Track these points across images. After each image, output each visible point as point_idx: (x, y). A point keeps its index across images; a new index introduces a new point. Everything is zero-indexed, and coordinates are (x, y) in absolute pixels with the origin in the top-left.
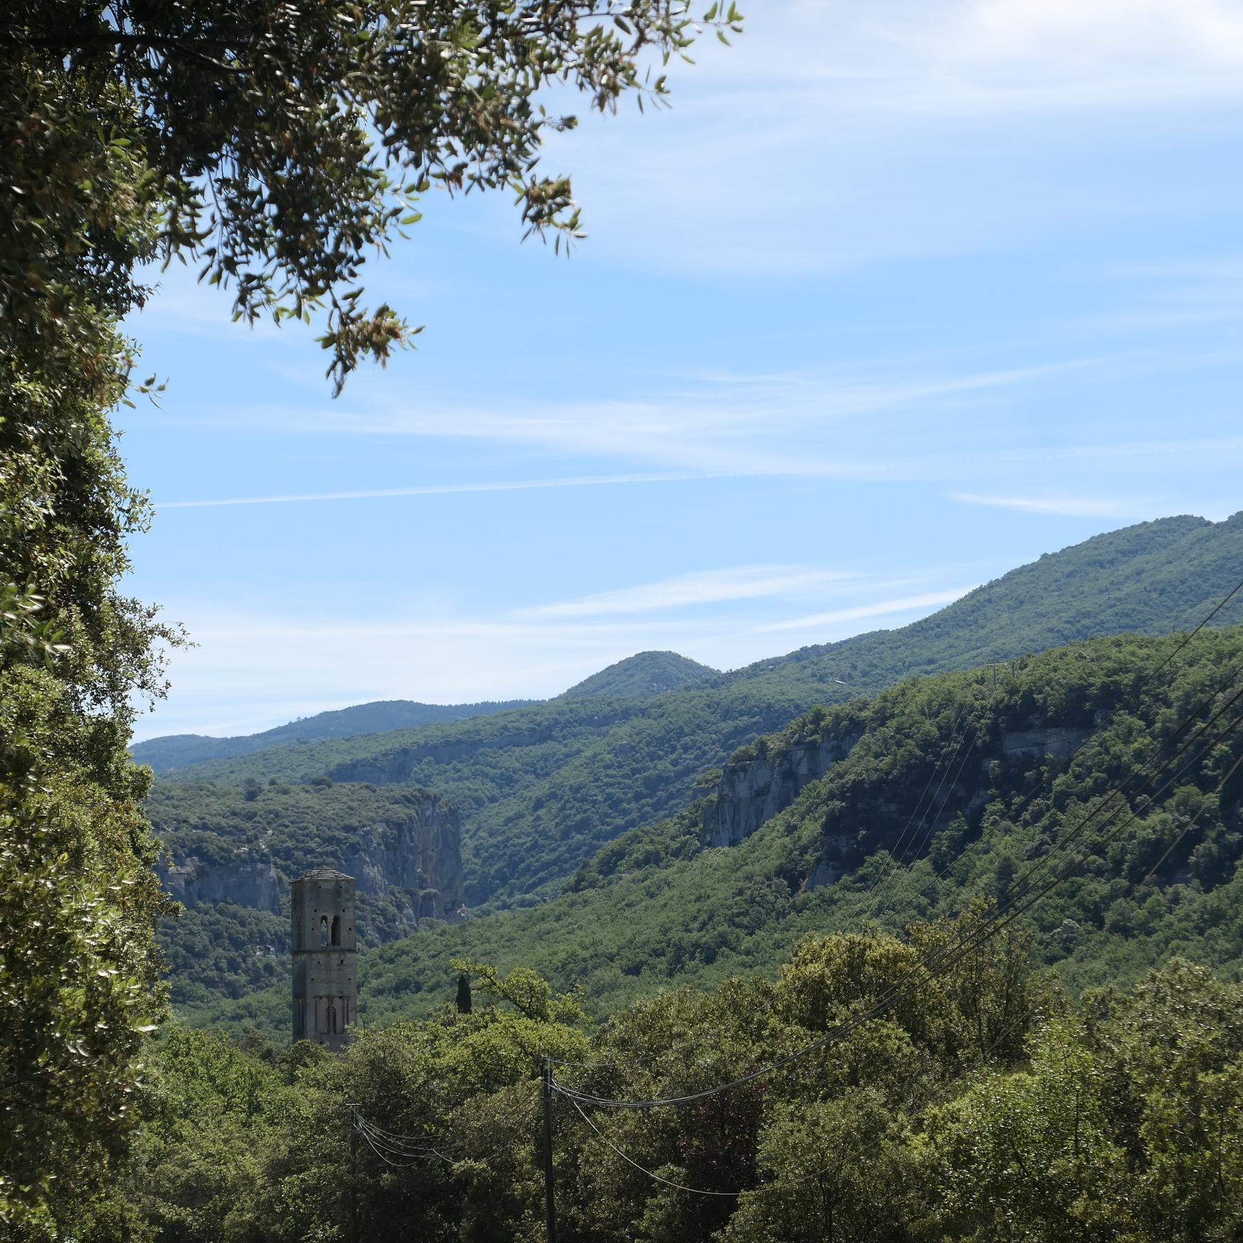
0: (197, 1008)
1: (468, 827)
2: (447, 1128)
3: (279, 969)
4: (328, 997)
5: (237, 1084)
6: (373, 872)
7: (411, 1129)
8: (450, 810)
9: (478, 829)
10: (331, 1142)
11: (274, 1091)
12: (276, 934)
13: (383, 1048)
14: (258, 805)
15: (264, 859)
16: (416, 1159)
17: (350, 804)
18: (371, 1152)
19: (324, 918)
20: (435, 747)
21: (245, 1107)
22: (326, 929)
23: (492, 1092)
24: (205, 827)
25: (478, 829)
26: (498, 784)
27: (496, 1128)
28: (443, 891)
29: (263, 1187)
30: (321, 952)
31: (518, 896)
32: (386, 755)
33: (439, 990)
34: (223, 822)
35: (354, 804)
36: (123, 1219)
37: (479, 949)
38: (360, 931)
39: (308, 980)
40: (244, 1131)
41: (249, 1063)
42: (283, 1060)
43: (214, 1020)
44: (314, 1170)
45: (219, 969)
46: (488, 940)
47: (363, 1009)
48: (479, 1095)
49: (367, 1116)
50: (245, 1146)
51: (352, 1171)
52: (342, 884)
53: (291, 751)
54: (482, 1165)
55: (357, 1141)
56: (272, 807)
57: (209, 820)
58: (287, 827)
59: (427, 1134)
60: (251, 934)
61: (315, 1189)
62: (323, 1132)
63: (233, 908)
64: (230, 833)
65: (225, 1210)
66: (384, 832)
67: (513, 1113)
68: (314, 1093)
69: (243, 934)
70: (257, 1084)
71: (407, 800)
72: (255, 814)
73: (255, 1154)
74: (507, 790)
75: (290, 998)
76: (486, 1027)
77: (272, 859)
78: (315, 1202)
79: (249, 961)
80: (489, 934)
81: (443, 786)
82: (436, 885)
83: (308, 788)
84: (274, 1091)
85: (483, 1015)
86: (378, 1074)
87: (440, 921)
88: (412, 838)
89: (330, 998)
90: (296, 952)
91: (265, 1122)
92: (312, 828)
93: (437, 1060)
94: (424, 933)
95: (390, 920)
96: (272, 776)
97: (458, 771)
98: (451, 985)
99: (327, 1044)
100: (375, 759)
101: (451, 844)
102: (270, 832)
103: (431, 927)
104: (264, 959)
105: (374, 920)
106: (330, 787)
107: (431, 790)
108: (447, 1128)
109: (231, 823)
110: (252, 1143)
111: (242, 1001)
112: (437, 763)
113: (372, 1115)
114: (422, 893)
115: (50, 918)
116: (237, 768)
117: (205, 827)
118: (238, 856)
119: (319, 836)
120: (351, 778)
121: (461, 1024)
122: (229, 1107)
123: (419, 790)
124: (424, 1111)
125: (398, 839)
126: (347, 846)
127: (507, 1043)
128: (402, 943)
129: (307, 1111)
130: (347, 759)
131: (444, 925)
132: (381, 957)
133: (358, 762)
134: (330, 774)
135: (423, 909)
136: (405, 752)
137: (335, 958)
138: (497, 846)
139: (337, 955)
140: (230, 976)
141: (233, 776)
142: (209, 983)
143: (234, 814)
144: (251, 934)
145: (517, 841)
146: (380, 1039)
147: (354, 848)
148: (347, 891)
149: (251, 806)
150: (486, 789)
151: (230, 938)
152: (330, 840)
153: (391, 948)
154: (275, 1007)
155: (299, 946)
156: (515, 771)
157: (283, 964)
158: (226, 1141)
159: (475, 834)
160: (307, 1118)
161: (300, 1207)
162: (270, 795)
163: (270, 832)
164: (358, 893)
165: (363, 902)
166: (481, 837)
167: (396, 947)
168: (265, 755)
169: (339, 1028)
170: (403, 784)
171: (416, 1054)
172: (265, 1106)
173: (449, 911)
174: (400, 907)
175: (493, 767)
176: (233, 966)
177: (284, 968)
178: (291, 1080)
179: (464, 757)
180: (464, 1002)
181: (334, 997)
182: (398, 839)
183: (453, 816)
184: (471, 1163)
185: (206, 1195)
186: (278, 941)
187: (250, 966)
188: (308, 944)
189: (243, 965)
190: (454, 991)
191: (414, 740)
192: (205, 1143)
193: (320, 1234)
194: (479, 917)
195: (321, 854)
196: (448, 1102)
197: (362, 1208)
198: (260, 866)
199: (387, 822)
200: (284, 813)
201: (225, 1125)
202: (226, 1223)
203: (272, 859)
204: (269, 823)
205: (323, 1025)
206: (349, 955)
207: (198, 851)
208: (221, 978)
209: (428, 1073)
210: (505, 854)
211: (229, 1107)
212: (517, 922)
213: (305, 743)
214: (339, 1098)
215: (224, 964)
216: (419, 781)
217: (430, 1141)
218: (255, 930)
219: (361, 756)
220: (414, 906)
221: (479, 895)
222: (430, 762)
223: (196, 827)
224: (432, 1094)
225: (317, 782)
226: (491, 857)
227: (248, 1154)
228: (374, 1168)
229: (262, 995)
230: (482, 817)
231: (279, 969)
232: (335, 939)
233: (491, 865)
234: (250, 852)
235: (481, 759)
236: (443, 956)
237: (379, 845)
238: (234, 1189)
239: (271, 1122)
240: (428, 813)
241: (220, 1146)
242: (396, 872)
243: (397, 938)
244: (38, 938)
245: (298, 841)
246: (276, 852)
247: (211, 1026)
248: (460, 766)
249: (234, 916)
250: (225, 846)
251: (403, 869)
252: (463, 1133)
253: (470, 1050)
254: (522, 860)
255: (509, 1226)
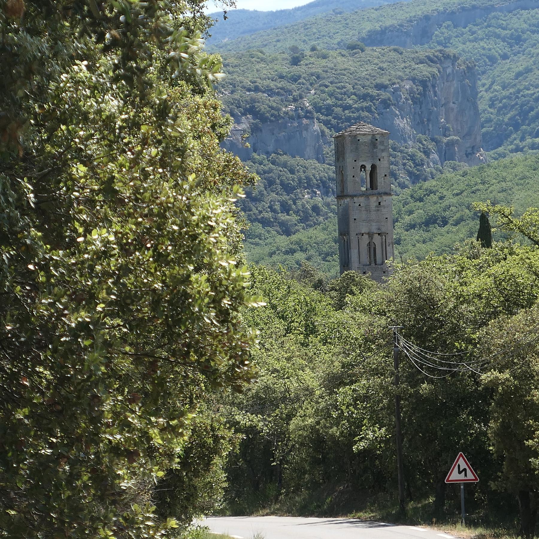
0: (257, 244)
1: (484, 81)
2: (475, 345)
3: (325, 209)
4: (368, 234)
5: (295, 310)
6: (403, 124)
7: (444, 345)
8: (468, 67)
9: (493, 83)
10: (375, 359)
11: (327, 316)
12: (321, 180)
13: (419, 279)
14: (300, 69)
15: (308, 115)
16: (450, 371)
17: (381, 65)
18: (411, 367)
19: (363, 167)
20: (453, 13)
21: (303, 329)
22: (365, 175)
23: (512, 314)
24: (257, 89)
25: (493, 83)
26: (509, 43)
27: (518, 345)
28: (464, 137)
29: (321, 397)
30: (362, 195)
31: (529, 140)
32: (411, 21)
33: (463, 223)
34: (272, 85)
35: (385, 65)
36: (213, 429)
37: (496, 187)
38: (394, 175)
39: (351, 220)
40: (303, 350)
41: (304, 292)
42: (333, 289)
43: (271, 255)
44: (364, 382)
45: (273, 211)
46: (504, 180)
47: (398, 242)
48: (501, 317)
49: (407, 336)
50: (304, 362)
51: (396, 383)
52: (378, 137)
53: (328, 20)
54: (506, 375)
55: (399, 357)
56: (313, 70)
57: (260, 83)
58: (327, 86)
59: (458, 351)
60: (300, 180)
61: (366, 398)
62: (370, 350)
63: (284, 158)
64: (278, 94)
65: (290, 417)
66: (411, 88)
67: (530, 332)
68: (364, 318)
69: (293, 180)
70: (312, 310)
71: (431, 60)
72: (299, 77)
73: (313, 369)
74: (516, 48)
75: (337, 234)
76: (505, 259)
77: (316, 115)
78: (365, 408)
79: (299, 203)
80: (505, 174)
81: (461, 47)
82: (457, 133)
83: (344, 52)
84: (327, 316)
85: (502, 249)
86: (415, 300)
87: (462, 163)
88: (435, 92)
89: (370, 235)
90: (340, 196)
91: (320, 342)
92: (349, 87)
93: (465, 288)
94: (448, 175)
95: (419, 164)
96: (313, 43)
97: (473, 33)
98: (473, 219)
99: (369, 274)
100: (401, 25)
101: (469, 97)
102: (313, 92)
103: (454, 169)
104: (312, 201)
105: (404, 164)
106: (363, 51)
107: (451, 51)
108: (475, 345)
109: (279, 85)
110: (311, 360)
111: (294, 238)
112: (455, 26)
113: (411, 335)
114: (445, 140)
115: (185, 223)
116: (281, 37)
117: (257, 89)
118: (286, 113)
119: (355, 94)
120: (380, 43)
121: (484, 257)
122: (288, 330)
123: (440, 51)
124: (455, 331)
125: (424, 94)
126: (379, 102)
127: (524, 272)
128: (430, 184)
129: (355, 333)
130: (377, 27)
131: (465, 167)
132: (412, 196)
133: (386, 28)
134: (363, 40)
135: (447, 154)
136: (427, 18)
137: (373, 200)
138: (509, 98)
139: (375, 198)
140: (283, 217)
141: (279, 44)
142: (265, 223)
143: (281, 77)
144: (300, 180)
145: (527, 92)
146: (416, 270)
147: (386, 104)
148: (382, 143)
149: (295, 70)
150: (498, 48)
151: (282, 184)
152: (364, 97)
153: (420, 189)
154: (323, 242)
155: (342, 191)
156: (523, 32)
157: (328, 205)
158: (288, 359)
159: (490, 88)
160: (357, 339)
161: (353, 413)
162: (312, 60)
163: (313, 92)
164: (391, 142)
165: (394, 149)
166: (495, 90)
167: (425, 187)
168: (306, 25)
169: (379, 261)
170: (426, 46)
171: (447, 284)
172: (320, 329)
173: (469, 155)
174: (427, 153)
175: (504, 29)
176: (286, 209)
177: (329, 208)
178: (340, 306)
179: (479, 21)
180: (485, 235)
181: (373, 234)
182: (424, 94)
183: (470, 72)
184: (496, 374)
185: (273, 405)
186: (323, 185)
187: (300, 207)
188: (350, 189)
189: (294, 207)
190: (476, 225)
191: (434, 7)
192: (271, 361)
193: (370, 435)
194: (496, 159)
195: (357, 110)
196: (475, 322)
197: (405, 413)
198: (305, 121)
199: (413, 79)
200: (324, 75)
201: (287, 345)
202: (291, 427)
203: (316, 115)
204: (311, 84)
205: (365, 259)
206: (385, 197)
207: (252, 110)
208: (276, 219)
209: (458, 298)
210: (516, 104)
211: (288, 330)
212: (529, 162)
213: (340, 13)
214: (383, 321)
215: (277, 207)
216: (439, 43)
217: (462, 356)
218: (303, 176)
219: (388, 23)
220: (439, 152)
221: (495, 140)
222: (449, 26)
223: (249, 90)
224: (461, 316)
225: (352, 47)
226: (505, 107)
227: (308, 370)
228: (414, 379)
229: (311, 232)
230: (496, 73)
231: (325, 209)
232: (373, 185)
233: (505, 114)
234: (296, 110)
235: (493, 21)
236: (465, 194)
237: (407, 99)
238: (298, 399)
239: (325, 342)
240: (449, 70)
241: (284, 363)
242: (422, 122)
243: (425, 180)
244: (174, 238)
245: (337, 99)
246: (318, 109)
247: (269, 260)
248: (475, 28)
249: (285, 165)
250: (274, 105)
251: (429, 120)
252: (489, 349)
253: (492, 278)
254: (532, 109)
255: (529, 426)
